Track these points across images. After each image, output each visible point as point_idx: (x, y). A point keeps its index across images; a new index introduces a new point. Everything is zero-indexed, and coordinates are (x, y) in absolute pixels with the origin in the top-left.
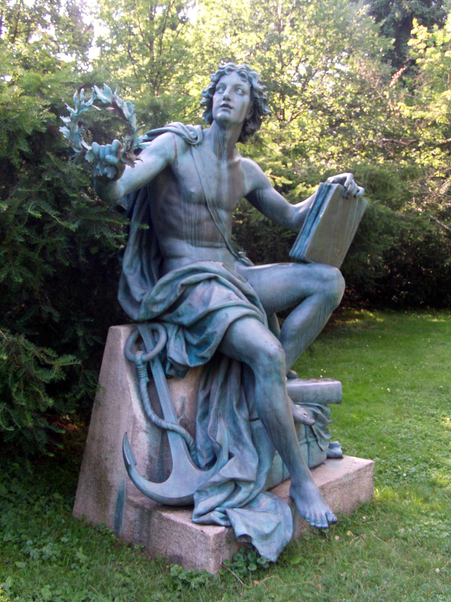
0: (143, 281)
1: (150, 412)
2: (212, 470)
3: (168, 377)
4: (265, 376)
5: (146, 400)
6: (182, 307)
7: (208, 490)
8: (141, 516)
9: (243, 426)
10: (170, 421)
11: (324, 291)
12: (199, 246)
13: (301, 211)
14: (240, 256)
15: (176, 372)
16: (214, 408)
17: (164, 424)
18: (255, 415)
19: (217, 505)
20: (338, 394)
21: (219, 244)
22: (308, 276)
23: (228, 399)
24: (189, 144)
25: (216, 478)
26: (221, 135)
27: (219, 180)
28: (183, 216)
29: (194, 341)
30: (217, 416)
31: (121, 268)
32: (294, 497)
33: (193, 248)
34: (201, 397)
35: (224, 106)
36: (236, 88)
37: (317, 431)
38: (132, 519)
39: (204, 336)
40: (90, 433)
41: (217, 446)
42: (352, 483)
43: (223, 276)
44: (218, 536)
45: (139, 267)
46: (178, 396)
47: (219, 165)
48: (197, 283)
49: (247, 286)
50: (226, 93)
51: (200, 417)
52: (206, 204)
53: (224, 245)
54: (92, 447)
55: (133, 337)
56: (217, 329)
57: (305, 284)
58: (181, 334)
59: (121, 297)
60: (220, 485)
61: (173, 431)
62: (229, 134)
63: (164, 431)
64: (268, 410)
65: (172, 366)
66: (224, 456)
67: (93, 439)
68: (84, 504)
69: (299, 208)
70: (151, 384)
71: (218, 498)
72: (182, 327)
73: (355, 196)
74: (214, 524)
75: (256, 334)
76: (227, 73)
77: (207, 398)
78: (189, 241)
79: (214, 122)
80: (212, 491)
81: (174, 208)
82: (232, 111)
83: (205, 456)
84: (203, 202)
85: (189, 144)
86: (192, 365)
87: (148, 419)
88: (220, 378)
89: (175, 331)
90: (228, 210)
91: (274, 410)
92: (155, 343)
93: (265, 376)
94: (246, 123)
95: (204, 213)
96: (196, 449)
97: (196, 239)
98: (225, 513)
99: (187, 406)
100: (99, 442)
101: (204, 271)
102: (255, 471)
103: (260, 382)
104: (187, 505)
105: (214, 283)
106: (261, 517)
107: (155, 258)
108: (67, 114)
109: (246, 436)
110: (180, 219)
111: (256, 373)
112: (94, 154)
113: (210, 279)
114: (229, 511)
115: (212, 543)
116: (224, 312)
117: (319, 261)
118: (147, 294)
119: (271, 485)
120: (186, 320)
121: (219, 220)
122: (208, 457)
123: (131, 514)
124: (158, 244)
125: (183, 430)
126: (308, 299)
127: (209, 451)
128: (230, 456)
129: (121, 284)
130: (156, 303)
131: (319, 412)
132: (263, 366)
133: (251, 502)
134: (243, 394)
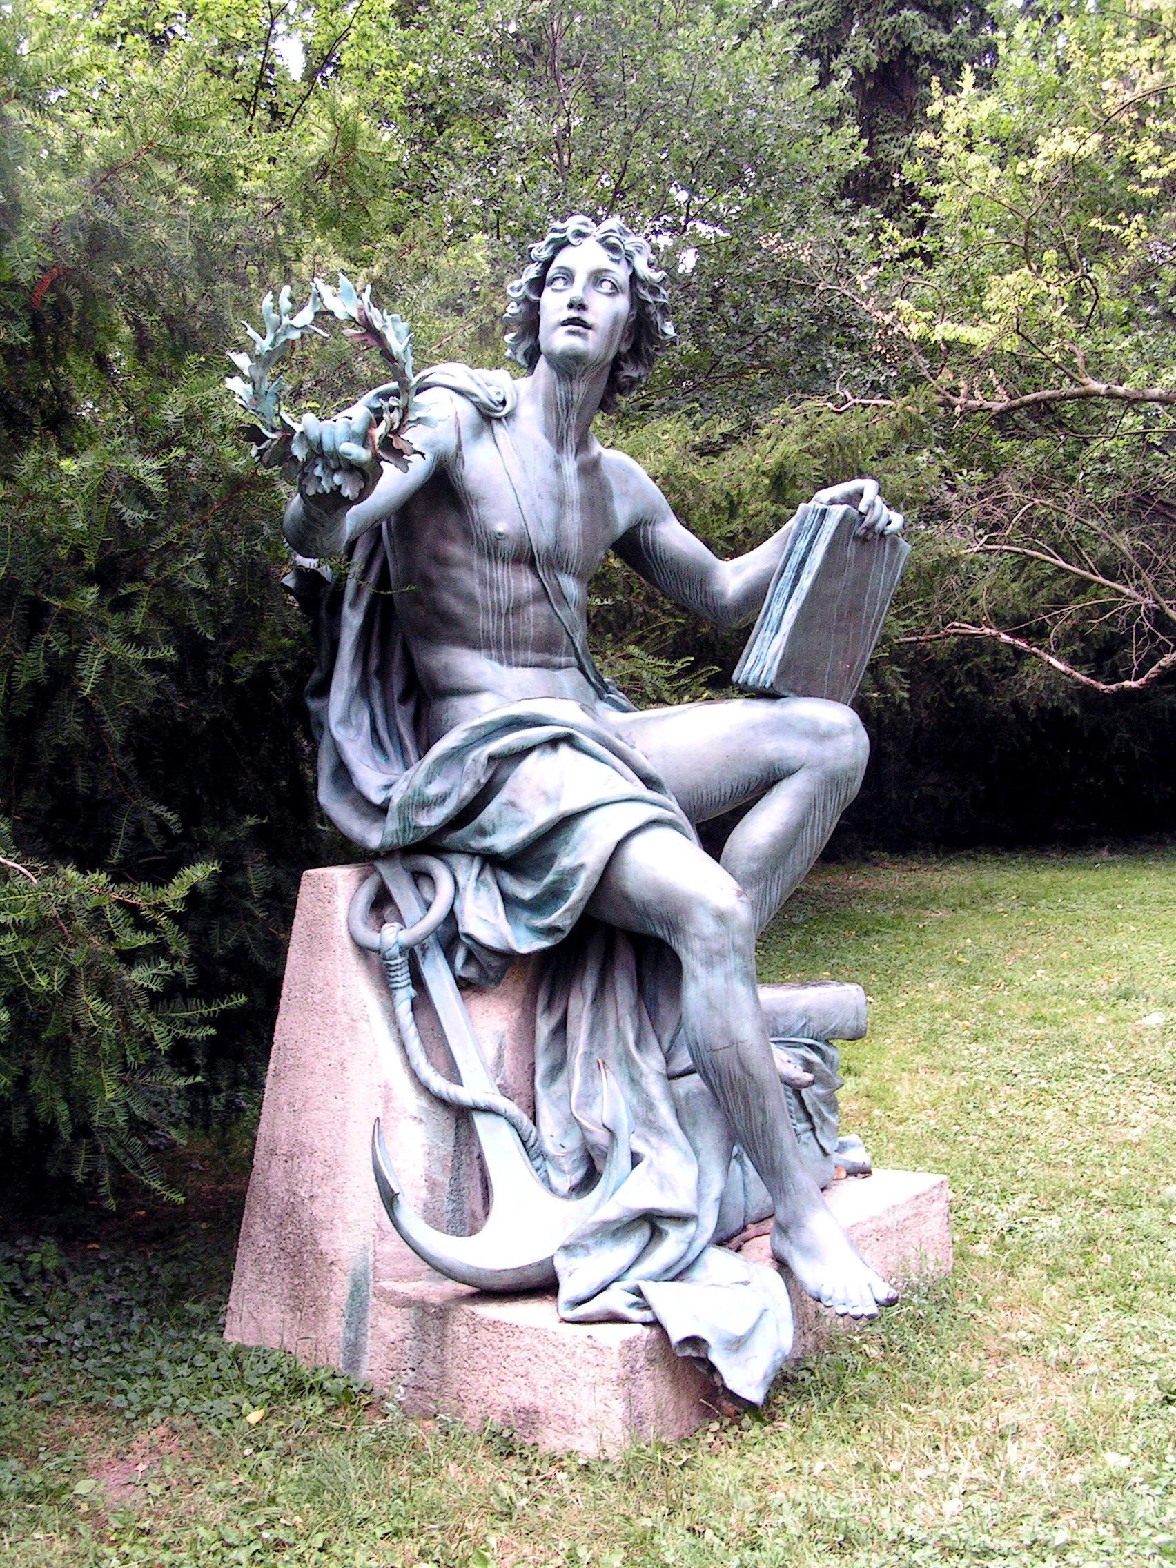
0: (380, 758)
3: (464, 985)
4: (709, 964)
7: (590, 1242)
8: (420, 1326)
9: (655, 1087)
10: (476, 1087)
12: (517, 665)
15: (484, 970)
16: (581, 1051)
19: (614, 1275)
20: (857, 1016)
21: (563, 660)
22: (784, 727)
23: (611, 1028)
24: (489, 416)
26: (561, 391)
27: (560, 501)
28: (478, 591)
29: (526, 892)
30: (595, 1066)
31: (322, 725)
32: (785, 1254)
33: (504, 670)
34: (544, 1027)
36: (597, 278)
37: (814, 1104)
38: (392, 1336)
39: (550, 877)
40: (261, 1144)
41: (600, 1137)
42: (902, 1229)
43: (585, 732)
44: (629, 1345)
45: (367, 722)
46: (481, 1032)
47: (558, 466)
48: (522, 754)
50: (576, 291)
51: (544, 1076)
52: (532, 564)
53: (573, 660)
54: (270, 1177)
55: (367, 892)
56: (585, 853)
57: (774, 748)
58: (488, 876)
59: (326, 796)
60: (618, 1230)
61: (488, 1110)
62: (580, 390)
63: (462, 1116)
64: (720, 1043)
65: (470, 957)
67: (272, 1153)
68: (256, 1313)
70: (422, 1001)
72: (492, 861)
73: (882, 534)
75: (670, 865)
76: (573, 241)
77: (561, 1029)
78: (494, 653)
79: (542, 364)
80: (599, 1244)
82: (590, 332)
83: (566, 1168)
84: (525, 557)
86: (524, 950)
88: (590, 983)
89: (475, 870)
91: (734, 1044)
94: (617, 364)
95: (527, 584)
96: (544, 1155)
97: (507, 648)
98: (638, 1292)
100: (290, 1157)
101: (535, 722)
102: (694, 1194)
103: (695, 978)
104: (542, 1285)
105: (564, 749)
107: (403, 700)
109: (665, 1112)
110: (470, 599)
111: (685, 957)
112: (309, 441)
114: (648, 1289)
115: (613, 1365)
116: (587, 823)
119: (722, 1235)
120: (503, 841)
122: (575, 1169)
123: (389, 1325)
124: (409, 662)
125: (512, 1108)
126: (784, 783)
127: (576, 1156)
129: (325, 765)
130: (427, 805)
131: (814, 1057)
132: (703, 939)
133: (690, 1267)
134: (646, 1017)
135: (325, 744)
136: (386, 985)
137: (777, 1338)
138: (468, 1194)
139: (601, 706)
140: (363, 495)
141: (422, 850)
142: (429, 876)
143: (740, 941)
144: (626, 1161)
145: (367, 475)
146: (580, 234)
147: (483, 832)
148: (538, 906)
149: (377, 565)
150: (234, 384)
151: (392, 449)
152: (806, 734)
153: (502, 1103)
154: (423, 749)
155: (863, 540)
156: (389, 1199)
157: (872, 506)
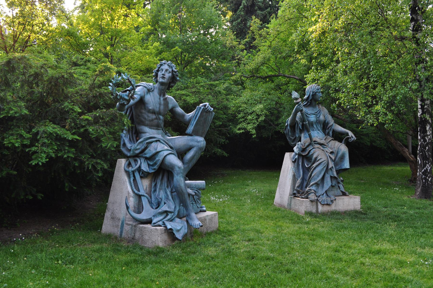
1: (135, 190)
2: (158, 209)
3: (141, 177)
5: (133, 185)
6: (147, 151)
9: (169, 193)
10: (142, 192)
11: (198, 146)
13: (190, 116)
14: (167, 133)
15: (144, 175)
17: (140, 193)
18: (174, 190)
22: (193, 140)
24: (149, 91)
25: (160, 211)
27: (160, 104)
28: (147, 118)
30: (160, 189)
33: (150, 130)
34: (153, 185)
35: (162, 77)
36: (167, 70)
41: (160, 200)
46: (144, 184)
47: (160, 99)
48: (152, 142)
49: (170, 144)
50: (163, 73)
55: (127, 162)
56: (160, 158)
57: (191, 143)
58: (146, 161)
60: (161, 213)
61: (144, 196)
63: (139, 197)
65: (142, 173)
66: (163, 203)
69: (189, 115)
70: (135, 180)
71: (161, 217)
72: (146, 159)
74: (160, 226)
75: (174, 160)
77: (156, 185)
81: (143, 114)
84: (154, 112)
85: (149, 91)
87: (134, 192)
88: (160, 177)
90: (163, 116)
91: (180, 187)
92: (136, 165)
93: (177, 175)
95: (154, 117)
96: (152, 203)
97: (151, 126)
99: (148, 188)
104: (149, 222)
105: (158, 142)
106: (176, 224)
108: (111, 82)
109: (170, 197)
110: (145, 119)
111: (174, 174)
113: (157, 141)
117: (197, 135)
118: (133, 146)
120: (148, 156)
121: (160, 119)
123: (127, 228)
128: (165, 203)
130: (137, 150)
131: (197, 192)
135: (122, 140)
136: (129, 177)
137: (184, 230)
138: (139, 209)
139: (166, 136)
140: (128, 104)
141: (136, 156)
142: (137, 161)
143: (182, 171)
144: (163, 203)
145: (129, 101)
146: (164, 63)
147: (145, 154)
148: (153, 165)
149: (131, 113)
150: (110, 87)
151: (132, 97)
152: (196, 141)
153: (145, 195)
154: (137, 141)
155: (206, 112)
156: (128, 208)
157: (208, 107)
